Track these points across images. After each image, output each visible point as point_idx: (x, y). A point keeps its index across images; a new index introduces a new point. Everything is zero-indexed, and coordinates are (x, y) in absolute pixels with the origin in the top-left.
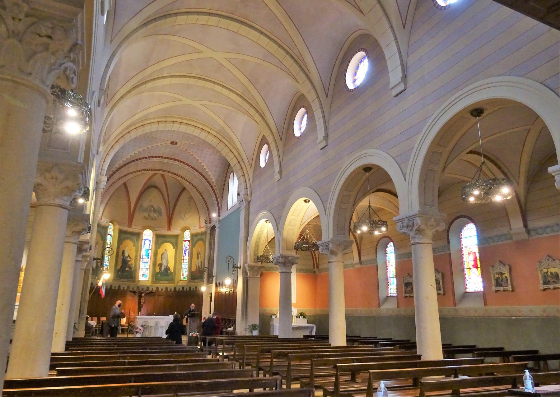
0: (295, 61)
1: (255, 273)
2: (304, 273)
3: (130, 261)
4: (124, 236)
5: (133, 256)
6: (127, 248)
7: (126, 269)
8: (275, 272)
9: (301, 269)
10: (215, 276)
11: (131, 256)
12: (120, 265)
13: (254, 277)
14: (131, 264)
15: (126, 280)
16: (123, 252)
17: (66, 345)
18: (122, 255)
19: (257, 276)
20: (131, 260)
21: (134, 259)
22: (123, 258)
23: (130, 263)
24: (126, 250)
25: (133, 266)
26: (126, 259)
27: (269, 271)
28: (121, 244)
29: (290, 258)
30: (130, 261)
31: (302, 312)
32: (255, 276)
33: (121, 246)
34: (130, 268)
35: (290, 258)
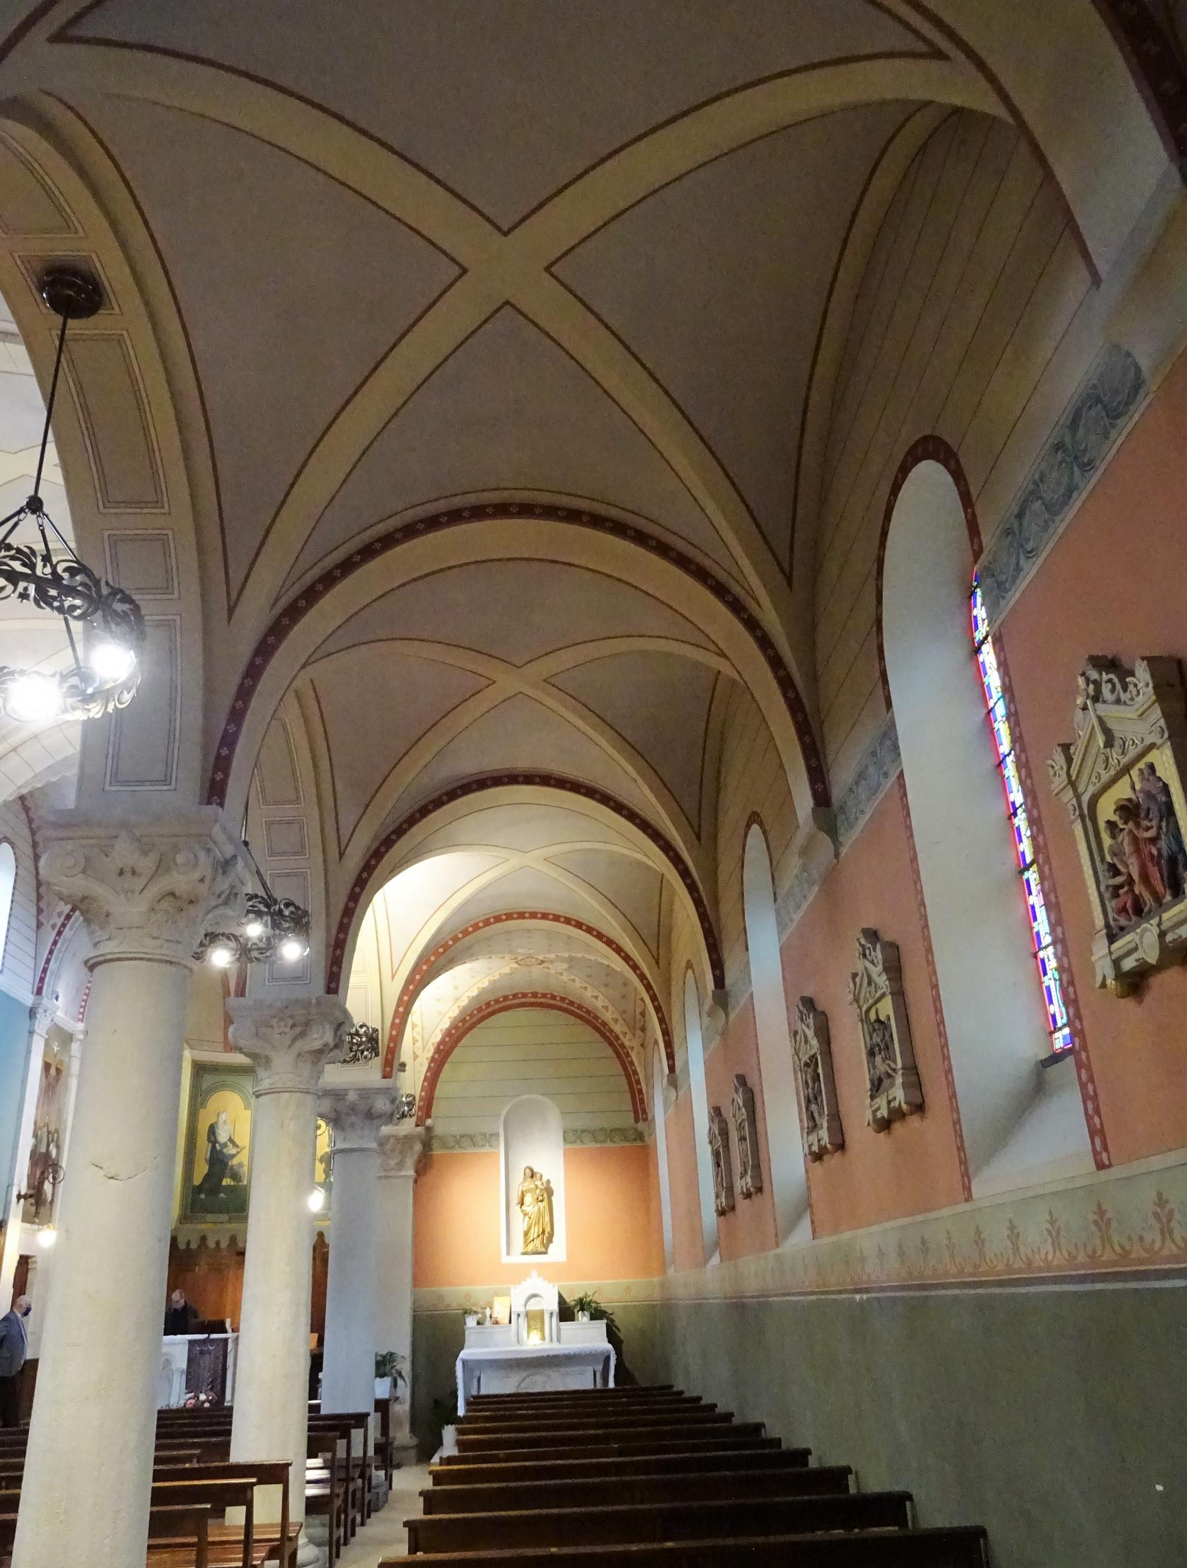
0: (733, 484)
1: (393, 1163)
2: (599, 1145)
3: (233, 1156)
4: (208, 1080)
5: (243, 1139)
6: (223, 1117)
7: (224, 1183)
8: (483, 1150)
9: (583, 1131)
10: (14, 1199)
11: (236, 1140)
12: (201, 1169)
13: (386, 1177)
14: (240, 1165)
15: (225, 1217)
16: (212, 1130)
17: (159, 1419)
18: (209, 1140)
19: (403, 1173)
20: (238, 1153)
21: (247, 1148)
22: (214, 1147)
23: (234, 1162)
24: (221, 1121)
25: (246, 1169)
26: (221, 1151)
27: (457, 1151)
28: (203, 1104)
29: (352, 1097)
30: (233, 1156)
31: (586, 1296)
32: (392, 1173)
33: (202, 1113)
34: (235, 1176)
35: (352, 1097)
